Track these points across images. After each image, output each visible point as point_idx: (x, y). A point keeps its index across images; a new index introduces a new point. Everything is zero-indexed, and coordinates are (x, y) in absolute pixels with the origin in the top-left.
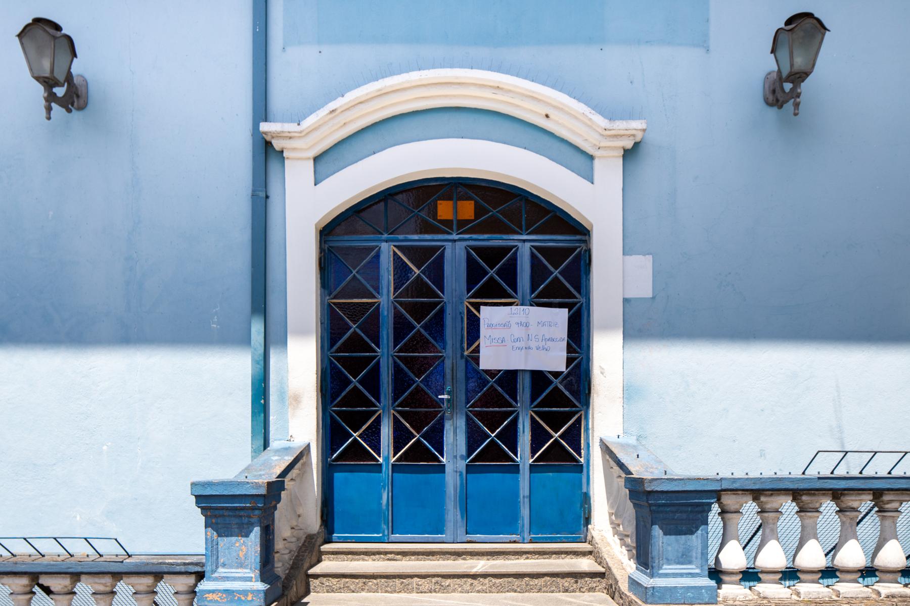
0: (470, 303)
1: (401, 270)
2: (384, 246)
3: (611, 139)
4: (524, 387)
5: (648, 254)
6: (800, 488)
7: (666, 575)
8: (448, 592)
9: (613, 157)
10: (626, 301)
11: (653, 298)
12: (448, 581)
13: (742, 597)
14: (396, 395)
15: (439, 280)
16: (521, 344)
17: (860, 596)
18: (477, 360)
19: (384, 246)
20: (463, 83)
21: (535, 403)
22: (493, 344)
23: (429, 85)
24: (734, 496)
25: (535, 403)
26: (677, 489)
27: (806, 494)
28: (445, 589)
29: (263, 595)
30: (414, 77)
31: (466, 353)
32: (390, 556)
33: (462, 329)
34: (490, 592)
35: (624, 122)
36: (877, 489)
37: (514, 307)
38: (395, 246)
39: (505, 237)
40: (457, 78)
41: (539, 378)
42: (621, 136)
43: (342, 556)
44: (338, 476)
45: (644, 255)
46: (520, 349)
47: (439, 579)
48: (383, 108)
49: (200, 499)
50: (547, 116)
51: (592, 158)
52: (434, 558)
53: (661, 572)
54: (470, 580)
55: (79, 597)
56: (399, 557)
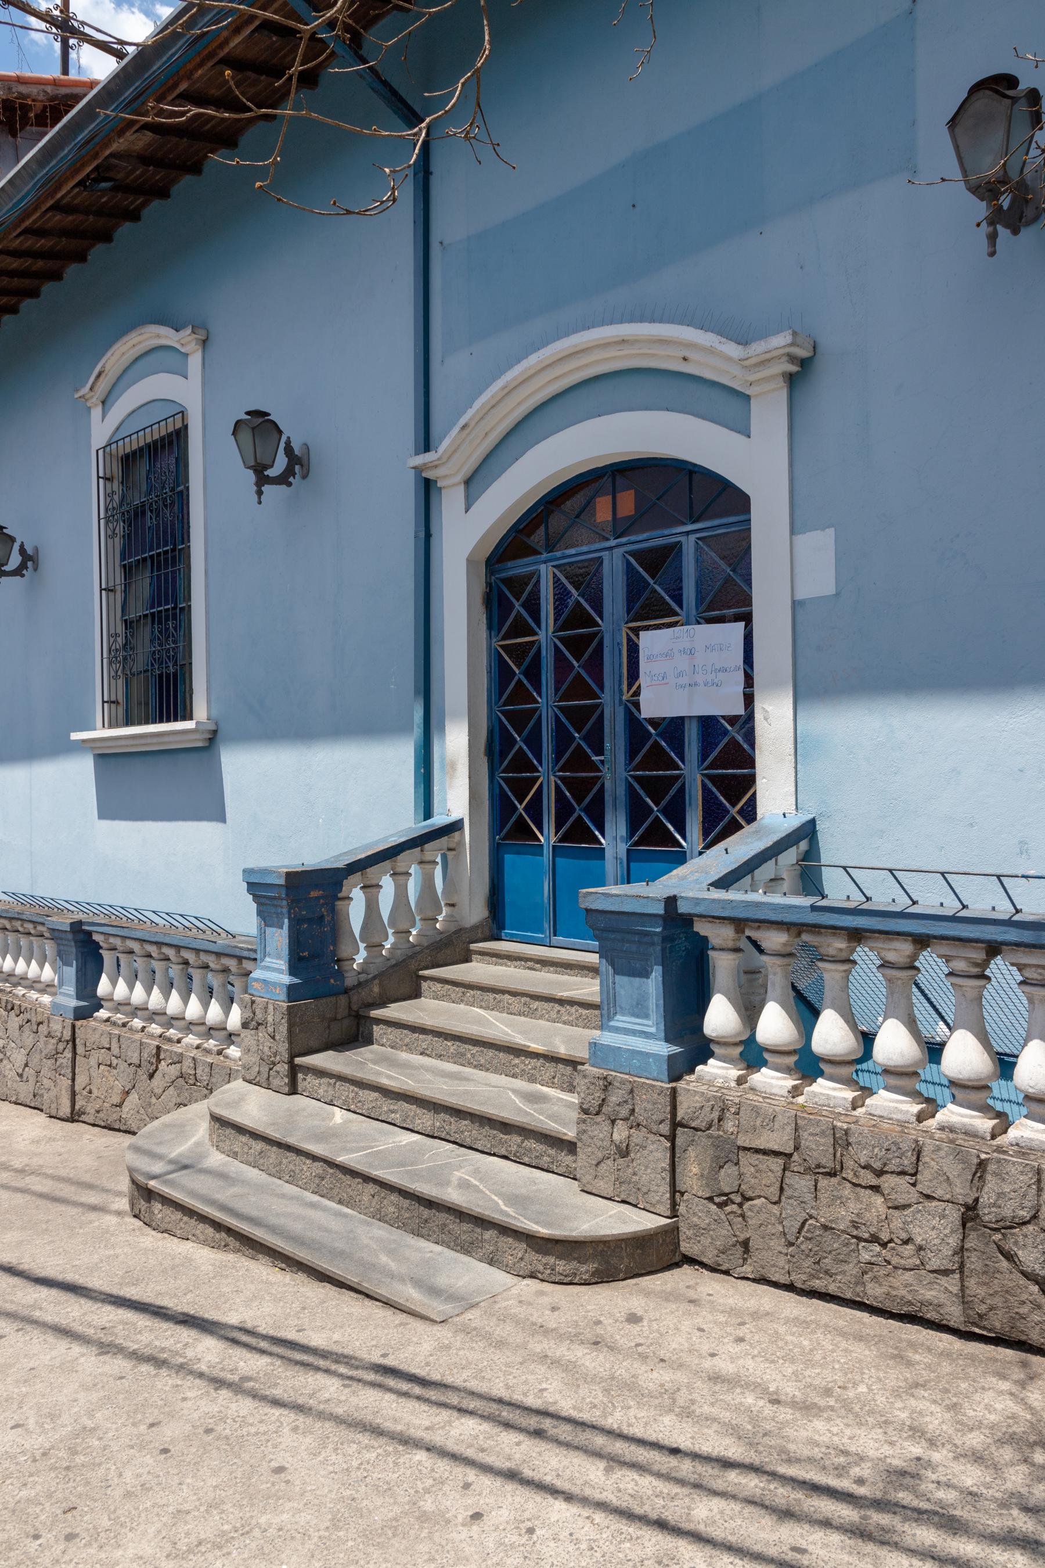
0: (630, 628)
1: (561, 596)
2: (543, 568)
3: (757, 369)
4: (692, 737)
5: (828, 527)
6: (785, 920)
7: (617, 1030)
8: (535, 1018)
9: (774, 390)
10: (796, 605)
11: (837, 595)
12: (536, 1004)
13: (721, 1080)
14: (558, 754)
15: (598, 605)
16: (684, 680)
17: (894, 1116)
18: (637, 705)
19: (543, 568)
20: (587, 349)
21: (706, 763)
22: (654, 682)
23: (554, 363)
24: (710, 925)
25: (706, 763)
26: (613, 908)
27: (808, 932)
28: (532, 1014)
29: (285, 989)
30: (533, 360)
31: (624, 698)
32: (530, 964)
33: (620, 665)
34: (577, 1026)
35: (763, 343)
36: (920, 935)
37: (677, 629)
38: (553, 566)
39: (666, 532)
40: (576, 346)
41: (708, 724)
42: (769, 360)
43: (487, 958)
44: (509, 858)
45: (823, 529)
46: (683, 687)
47: (528, 999)
48: (519, 404)
49: (252, 887)
50: (685, 359)
51: (748, 398)
52: (572, 972)
53: (612, 1023)
54: (557, 1007)
55: (860, 970)
56: (538, 966)
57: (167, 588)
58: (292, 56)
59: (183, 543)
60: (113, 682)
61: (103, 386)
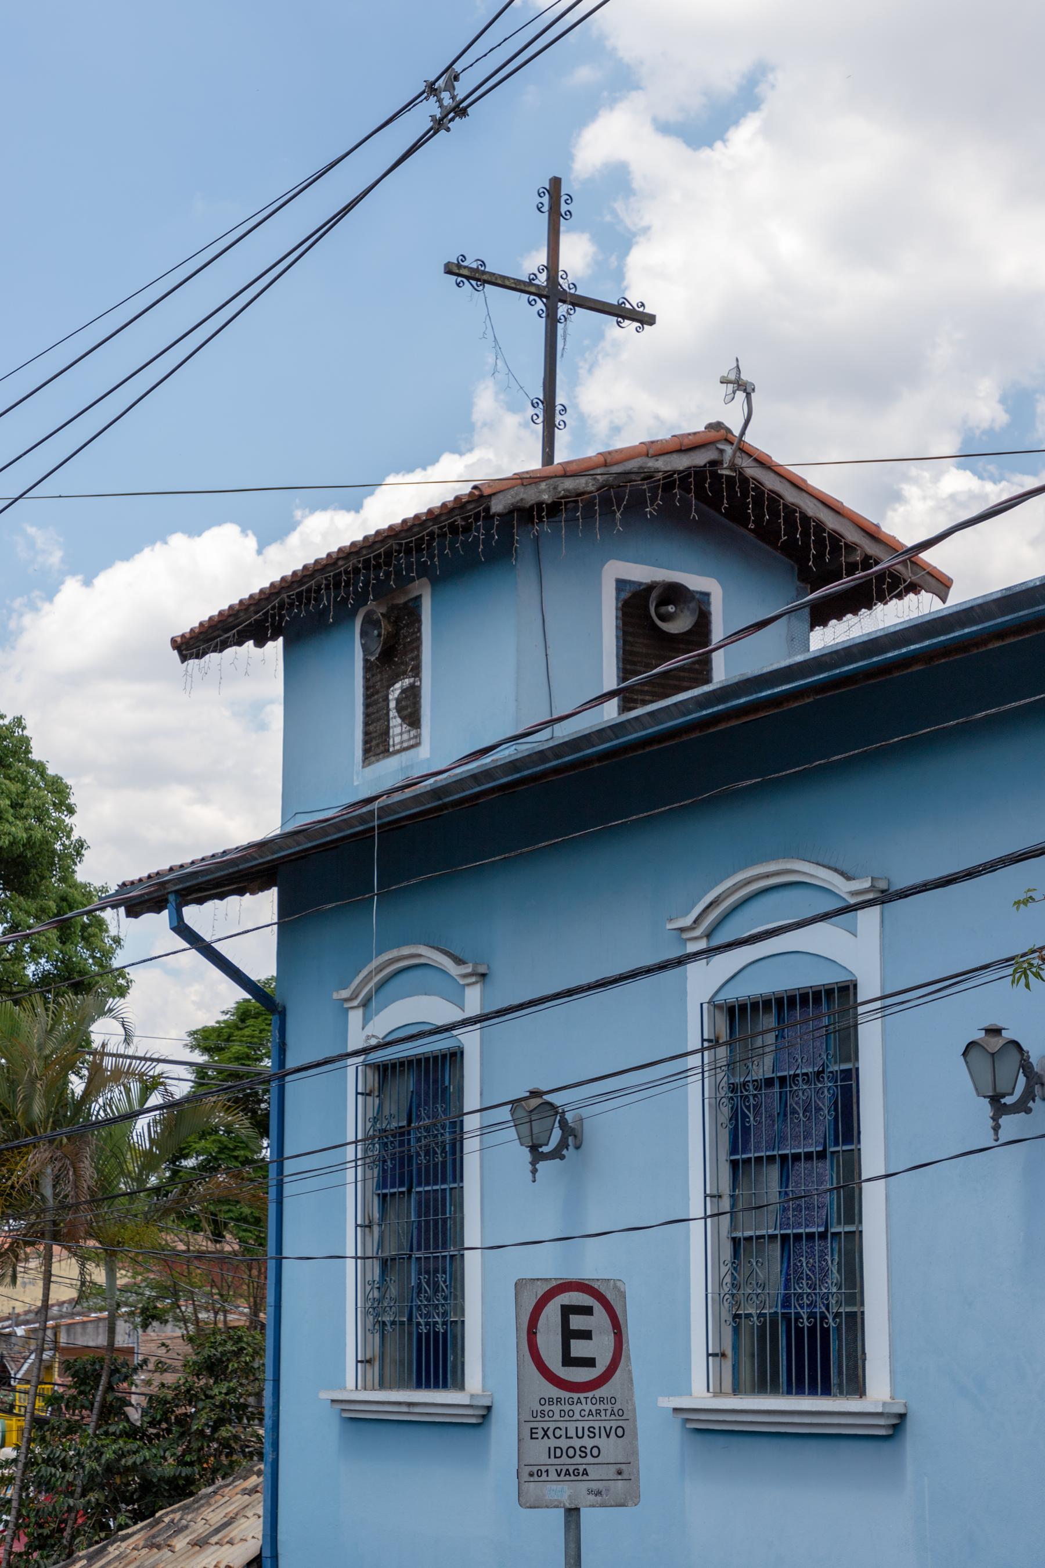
57: (436, 1235)
58: (642, 669)
59: (454, 1181)
60: (369, 1336)
61: (507, 752)
